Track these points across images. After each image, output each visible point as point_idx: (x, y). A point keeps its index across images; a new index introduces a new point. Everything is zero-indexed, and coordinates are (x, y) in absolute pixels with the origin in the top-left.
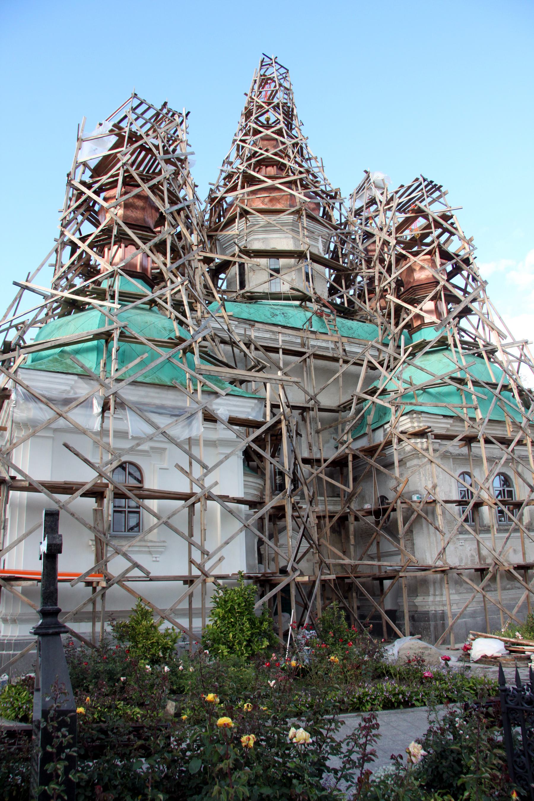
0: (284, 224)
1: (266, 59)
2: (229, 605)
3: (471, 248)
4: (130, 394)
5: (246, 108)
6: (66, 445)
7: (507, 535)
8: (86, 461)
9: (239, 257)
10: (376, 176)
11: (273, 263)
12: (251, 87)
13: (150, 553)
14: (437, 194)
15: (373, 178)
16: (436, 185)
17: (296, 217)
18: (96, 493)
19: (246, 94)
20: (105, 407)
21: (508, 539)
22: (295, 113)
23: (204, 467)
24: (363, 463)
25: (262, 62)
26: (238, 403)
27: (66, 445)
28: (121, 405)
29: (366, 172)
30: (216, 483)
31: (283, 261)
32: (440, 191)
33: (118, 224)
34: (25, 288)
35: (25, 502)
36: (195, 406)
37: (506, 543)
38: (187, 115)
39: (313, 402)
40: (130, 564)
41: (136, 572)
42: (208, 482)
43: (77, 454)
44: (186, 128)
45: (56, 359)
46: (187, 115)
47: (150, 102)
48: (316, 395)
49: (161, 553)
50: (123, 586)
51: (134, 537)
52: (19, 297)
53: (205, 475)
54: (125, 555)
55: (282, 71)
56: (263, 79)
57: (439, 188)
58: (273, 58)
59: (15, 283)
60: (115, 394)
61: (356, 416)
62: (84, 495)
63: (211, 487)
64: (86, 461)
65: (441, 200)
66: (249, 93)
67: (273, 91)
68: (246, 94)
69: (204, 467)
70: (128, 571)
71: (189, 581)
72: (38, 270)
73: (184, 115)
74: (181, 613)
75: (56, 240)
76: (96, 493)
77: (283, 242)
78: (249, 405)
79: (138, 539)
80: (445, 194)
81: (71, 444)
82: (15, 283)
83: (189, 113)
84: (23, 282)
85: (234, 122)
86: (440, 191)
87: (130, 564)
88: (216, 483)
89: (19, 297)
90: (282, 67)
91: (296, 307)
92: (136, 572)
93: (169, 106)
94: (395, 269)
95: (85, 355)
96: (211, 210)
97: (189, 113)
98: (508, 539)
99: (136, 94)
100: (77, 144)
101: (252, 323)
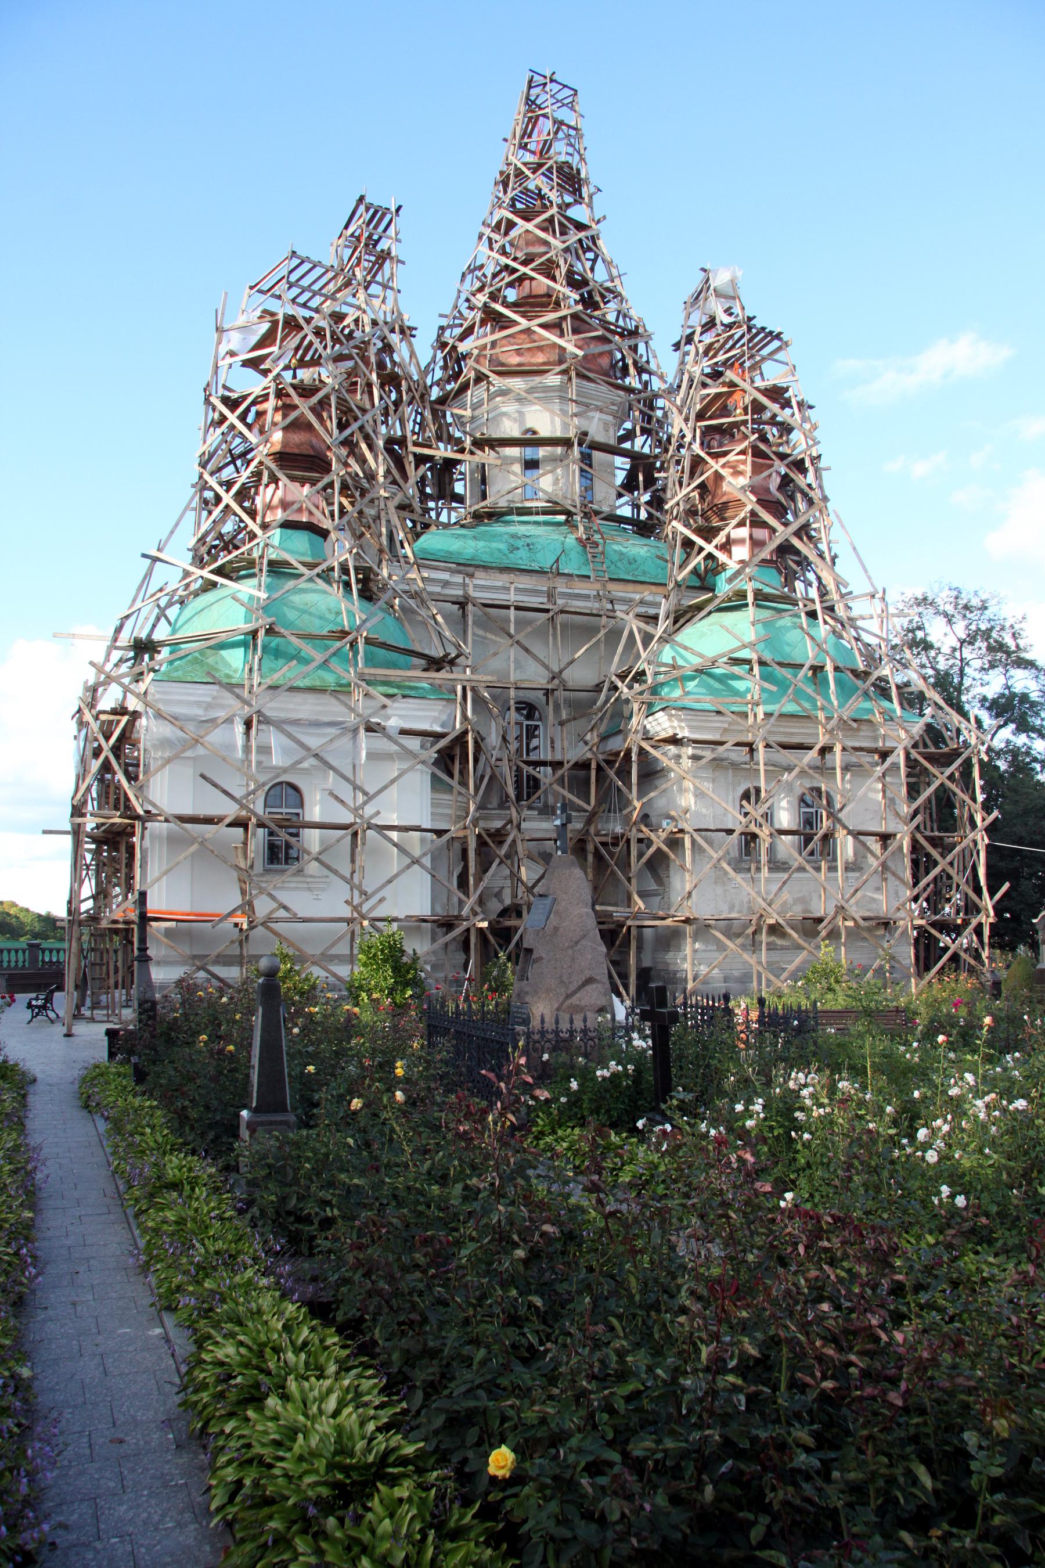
0: (547, 389)
1: (536, 78)
2: (373, 951)
3: (811, 443)
4: (278, 707)
5: (502, 173)
6: (203, 776)
7: (786, 876)
8: (226, 792)
9: (472, 453)
10: (720, 279)
11: (529, 453)
12: (512, 129)
13: (309, 889)
14: (776, 344)
15: (713, 284)
16: (771, 333)
17: (566, 378)
18: (240, 823)
19: (506, 140)
20: (248, 724)
21: (784, 883)
22: (583, 176)
23: (365, 793)
24: (616, 773)
25: (531, 81)
26: (409, 713)
27: (203, 776)
28: (264, 720)
29: (704, 270)
30: (378, 813)
31: (542, 452)
32: (780, 340)
33: (268, 468)
34: (155, 559)
35: (165, 833)
36: (358, 719)
37: (780, 889)
38: (398, 210)
39: (556, 681)
40: (275, 905)
41: (282, 913)
42: (369, 810)
43: (215, 785)
44: (397, 234)
45: (196, 658)
46: (398, 210)
47: (315, 258)
48: (561, 672)
49: (323, 890)
50: (268, 928)
51: (284, 871)
52: (149, 574)
53: (365, 803)
54: (270, 895)
55: (567, 92)
56: (530, 118)
57: (778, 337)
58: (548, 75)
59: (144, 556)
60: (259, 712)
61: (600, 709)
62: (230, 825)
63: (372, 817)
64: (226, 792)
65: (779, 356)
66: (509, 137)
67: (546, 141)
68: (506, 140)
69: (365, 793)
70: (272, 912)
71: (349, 921)
72: (172, 532)
73: (393, 209)
74: (339, 959)
75: (193, 486)
76: (240, 823)
77: (546, 421)
78: (427, 713)
79: (289, 873)
80: (786, 344)
81: (208, 775)
82: (144, 556)
83: (400, 207)
84: (154, 553)
85: (480, 201)
86: (780, 340)
87: (275, 905)
88: (378, 813)
89: (149, 574)
90: (565, 86)
91: (558, 524)
92: (282, 913)
93: (368, 200)
94: (713, 461)
95: (230, 651)
96: (445, 358)
97: (400, 207)
98: (784, 883)
99: (294, 252)
100: (216, 335)
101: (471, 570)
